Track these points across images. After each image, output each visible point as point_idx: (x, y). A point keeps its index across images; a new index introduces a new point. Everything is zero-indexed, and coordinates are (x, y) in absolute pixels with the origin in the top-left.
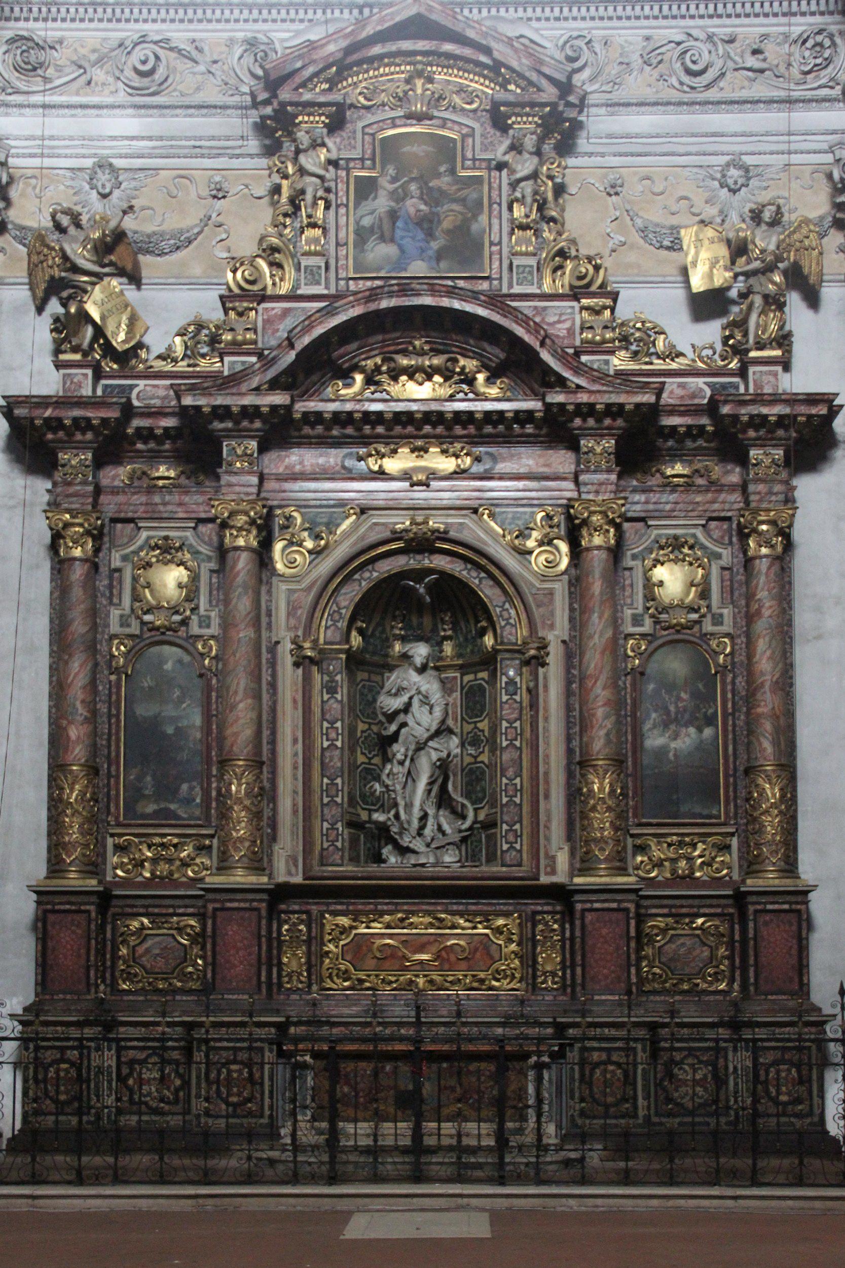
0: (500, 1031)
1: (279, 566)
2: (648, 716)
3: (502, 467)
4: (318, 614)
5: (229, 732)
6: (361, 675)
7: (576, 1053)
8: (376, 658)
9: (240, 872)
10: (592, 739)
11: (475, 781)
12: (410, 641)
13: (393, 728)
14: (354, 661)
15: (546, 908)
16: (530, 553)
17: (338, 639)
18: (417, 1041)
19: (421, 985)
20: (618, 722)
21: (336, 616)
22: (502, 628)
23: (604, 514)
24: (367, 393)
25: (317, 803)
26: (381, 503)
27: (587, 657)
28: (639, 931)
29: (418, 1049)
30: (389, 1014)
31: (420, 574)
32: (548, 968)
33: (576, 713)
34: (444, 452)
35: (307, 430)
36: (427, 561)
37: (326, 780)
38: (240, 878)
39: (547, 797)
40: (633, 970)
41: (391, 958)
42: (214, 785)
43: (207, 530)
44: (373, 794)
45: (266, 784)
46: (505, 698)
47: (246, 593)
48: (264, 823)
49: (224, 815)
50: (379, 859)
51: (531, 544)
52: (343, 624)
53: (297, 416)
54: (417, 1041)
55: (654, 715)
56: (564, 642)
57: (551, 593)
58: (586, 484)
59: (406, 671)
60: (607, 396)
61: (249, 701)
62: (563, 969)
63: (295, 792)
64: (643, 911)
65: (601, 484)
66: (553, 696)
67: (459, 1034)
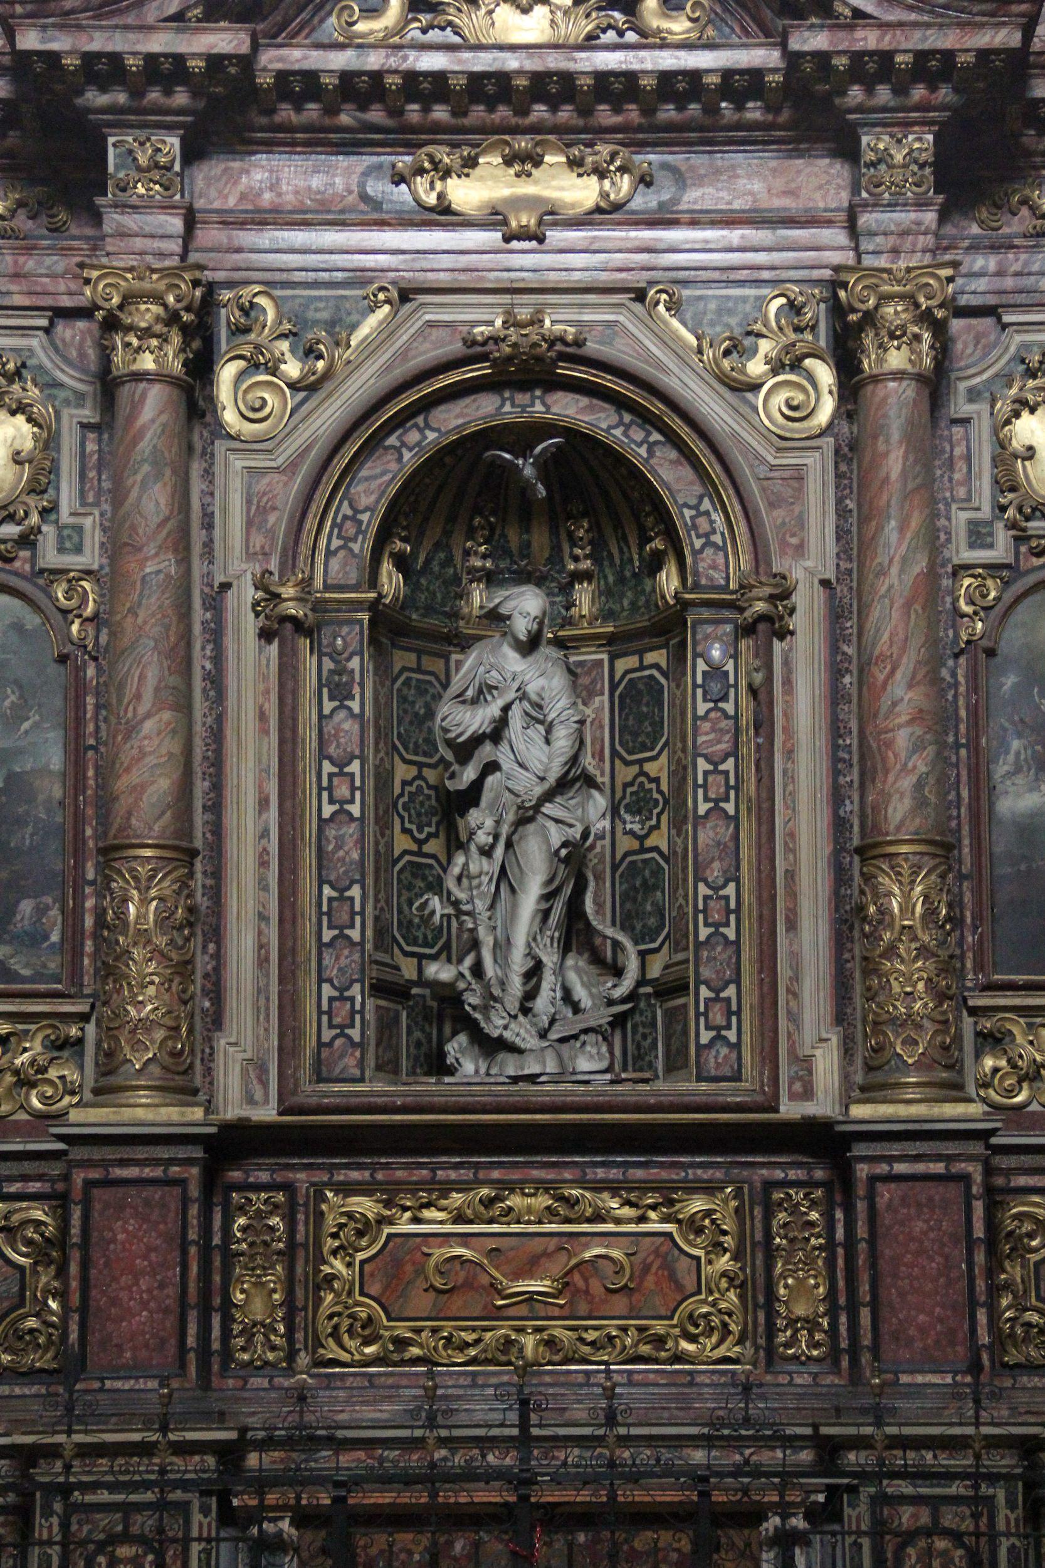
0: (698, 1456)
1: (230, 417)
2: (1004, 747)
3: (696, 197)
4: (311, 523)
5: (122, 784)
6: (402, 659)
7: (863, 1508)
8: (433, 621)
9: (144, 1097)
10: (886, 797)
11: (643, 888)
12: (502, 583)
13: (469, 774)
14: (388, 628)
15: (793, 1174)
16: (755, 387)
17: (353, 578)
18: (523, 1481)
19: (529, 1352)
20: (940, 757)
22: (695, 553)
23: (910, 299)
24: (414, 33)
27: (875, 614)
28: (992, 1225)
29: (524, 1498)
30: (463, 1418)
31: (523, 436)
32: (800, 1311)
33: (853, 741)
34: (574, 164)
35: (286, 113)
36: (539, 407)
37: (327, 891)
38: (146, 1111)
39: (792, 925)
40: (982, 1317)
41: (461, 1285)
42: (89, 903)
43: (71, 332)
44: (427, 920)
45: (202, 901)
46: (702, 708)
47: (158, 476)
48: (196, 988)
49: (111, 969)
51: (756, 367)
52: (362, 546)
53: (265, 80)
54: (523, 1481)
55: (1016, 744)
56: (825, 583)
57: (798, 476)
58: (872, 234)
59: (495, 650)
60: (918, 34)
61: (167, 715)
62: (833, 1312)
64: (1000, 1181)
65: (904, 233)
66: (804, 706)
67: (612, 1464)
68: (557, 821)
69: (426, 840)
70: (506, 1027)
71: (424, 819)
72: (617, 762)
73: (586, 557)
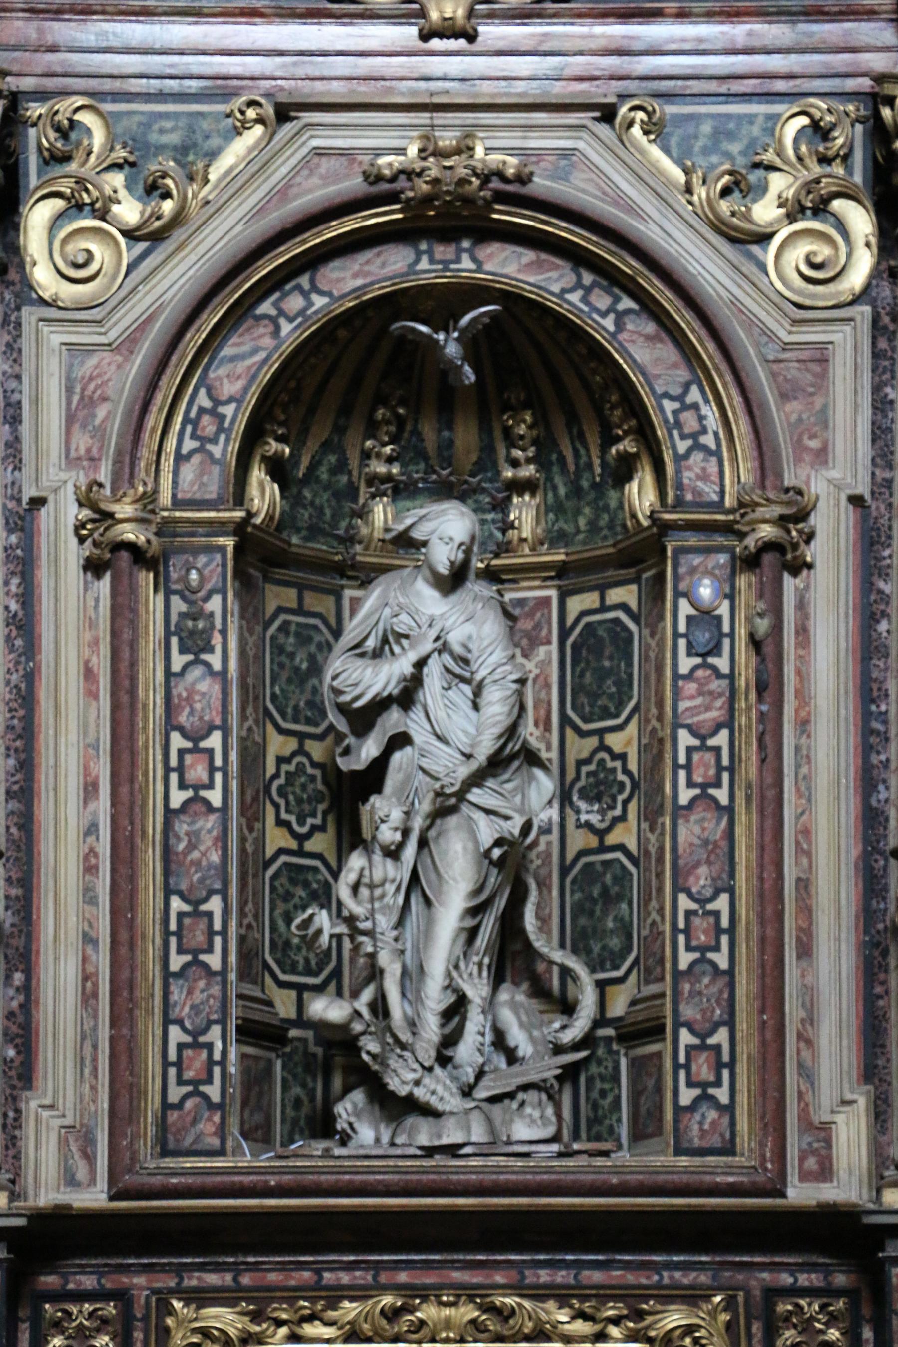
1: (43, 277)
4: (155, 419)
6: (278, 597)
11: (600, 895)
13: (370, 749)
14: (259, 555)
15: (803, 1279)
16: (764, 238)
17: (212, 492)
21: (208, 425)
22: (679, 459)
25: (154, 970)
26: (337, 91)
36: (467, 263)
37: (176, 904)
39: (805, 950)
46: (686, 663)
50: (323, 1126)
51: (765, 211)
52: (225, 449)
56: (856, 501)
57: (821, 357)
63: (89, 940)
68: (488, 812)
69: (308, 836)
70: (417, 1083)
71: (307, 807)
72: (569, 732)
73: (529, 461)
